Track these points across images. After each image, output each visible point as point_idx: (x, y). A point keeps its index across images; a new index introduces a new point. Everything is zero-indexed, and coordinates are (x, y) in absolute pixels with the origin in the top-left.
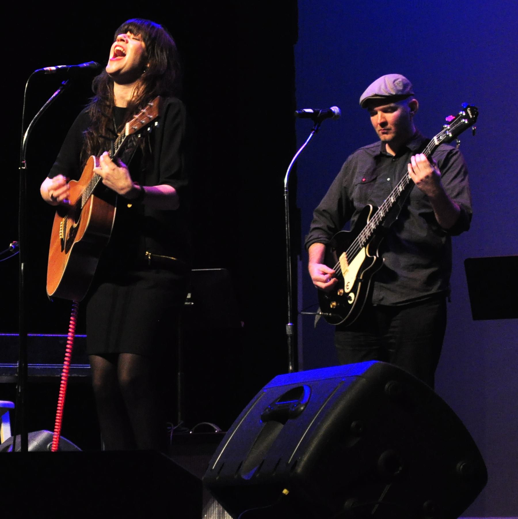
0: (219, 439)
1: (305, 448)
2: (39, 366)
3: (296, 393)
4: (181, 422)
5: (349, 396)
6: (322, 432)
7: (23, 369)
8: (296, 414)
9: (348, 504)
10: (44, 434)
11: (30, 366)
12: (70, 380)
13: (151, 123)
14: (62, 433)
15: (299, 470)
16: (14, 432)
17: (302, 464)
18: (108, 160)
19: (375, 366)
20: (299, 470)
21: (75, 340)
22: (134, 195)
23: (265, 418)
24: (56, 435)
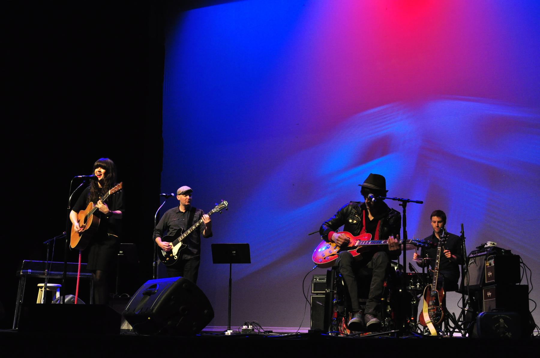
0: (129, 299)
1: (156, 305)
2: (70, 273)
3: (154, 286)
4: (117, 293)
5: (171, 288)
6: (162, 299)
7: (65, 275)
8: (154, 293)
9: (169, 323)
10: (71, 296)
11: (67, 273)
12: (80, 278)
13: (119, 191)
14: (78, 296)
15: (154, 311)
16: (61, 295)
17: (155, 309)
18: (101, 202)
19: (180, 279)
20: (154, 311)
21: (81, 265)
22: (110, 214)
23: (144, 294)
24: (76, 297)
